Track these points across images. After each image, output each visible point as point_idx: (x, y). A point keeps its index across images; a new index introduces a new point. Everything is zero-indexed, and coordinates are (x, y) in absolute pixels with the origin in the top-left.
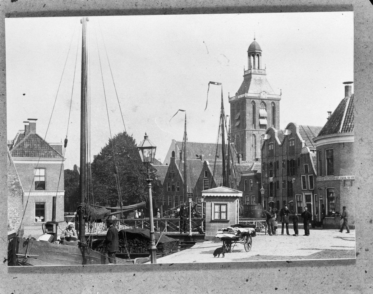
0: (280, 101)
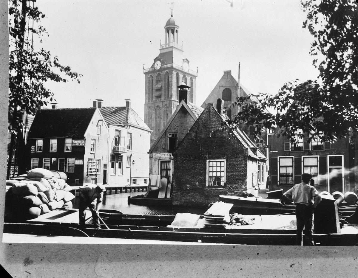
0: (196, 77)
